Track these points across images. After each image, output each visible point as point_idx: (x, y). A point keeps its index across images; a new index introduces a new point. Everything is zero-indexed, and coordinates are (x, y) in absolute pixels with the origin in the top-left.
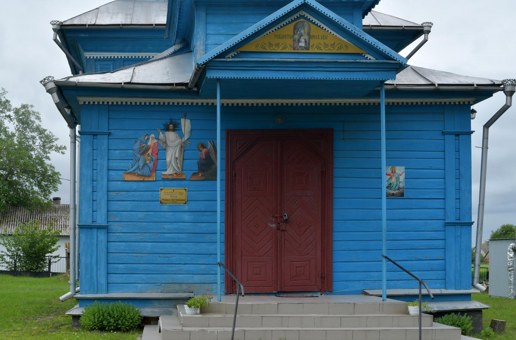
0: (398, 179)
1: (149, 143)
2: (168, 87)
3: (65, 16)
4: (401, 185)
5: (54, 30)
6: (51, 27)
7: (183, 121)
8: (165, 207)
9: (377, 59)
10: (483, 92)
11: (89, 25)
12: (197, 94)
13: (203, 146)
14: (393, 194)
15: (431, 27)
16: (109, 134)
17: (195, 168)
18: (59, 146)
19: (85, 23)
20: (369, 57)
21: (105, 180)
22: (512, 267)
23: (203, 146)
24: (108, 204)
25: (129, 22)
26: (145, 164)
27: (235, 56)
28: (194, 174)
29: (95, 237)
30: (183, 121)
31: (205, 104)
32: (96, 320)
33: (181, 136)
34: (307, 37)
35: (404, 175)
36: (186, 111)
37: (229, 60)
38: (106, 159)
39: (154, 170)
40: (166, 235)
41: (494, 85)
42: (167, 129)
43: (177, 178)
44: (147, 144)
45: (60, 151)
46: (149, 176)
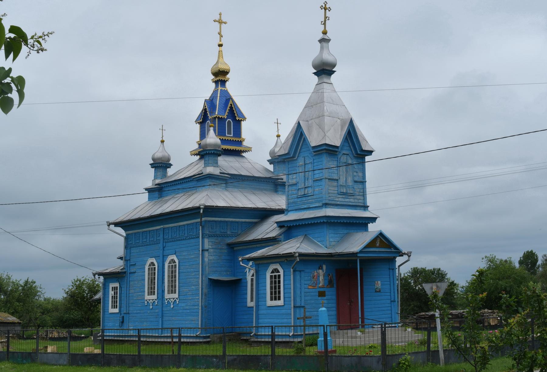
39: (316, 284)
42: (319, 269)
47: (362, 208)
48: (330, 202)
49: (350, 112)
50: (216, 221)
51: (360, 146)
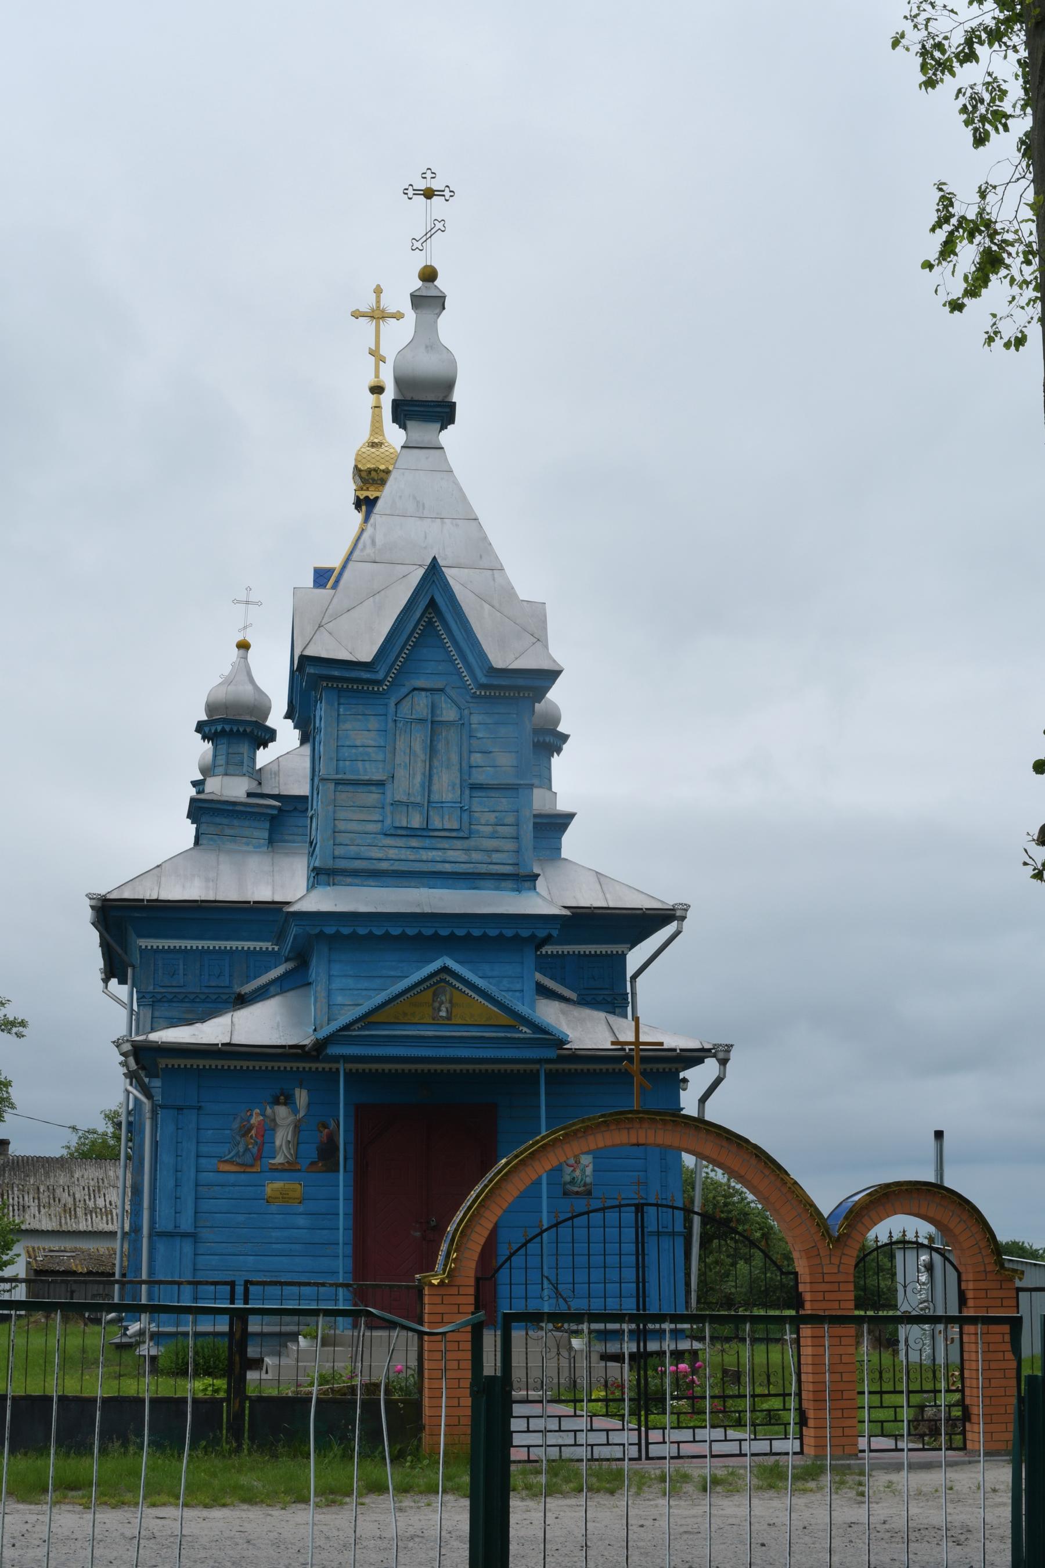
0: (583, 1171)
1: (253, 1121)
2: (279, 1051)
3: (111, 882)
4: (588, 1180)
5: (92, 907)
6: (88, 902)
7: (297, 1091)
8: (273, 1208)
9: (534, 1033)
10: (693, 1058)
11: (148, 901)
12: (316, 1059)
13: (325, 1126)
14: (577, 1193)
15: (686, 910)
16: (199, 1108)
17: (314, 1155)
18: (11, 1019)
19: (141, 897)
20: (525, 1029)
21: (193, 1170)
22: (925, 1301)
23: (325, 1126)
24: (196, 1203)
25: (211, 897)
26: (247, 1150)
27: (359, 1029)
28: (312, 1163)
29: (178, 1247)
30: (297, 1091)
31: (327, 1069)
32: (180, 1361)
33: (295, 1111)
34: (448, 1005)
35: (591, 1167)
36: (301, 1079)
37: (354, 1033)
38: (195, 1141)
39: (259, 1157)
40: (274, 1246)
41: (703, 1050)
42: (277, 1102)
43: (288, 1169)
44: (249, 1121)
45: (14, 1030)
46: (252, 1166)
47: (509, 884)
48: (342, 864)
49: (492, 538)
50: (185, 951)
51: (482, 655)
